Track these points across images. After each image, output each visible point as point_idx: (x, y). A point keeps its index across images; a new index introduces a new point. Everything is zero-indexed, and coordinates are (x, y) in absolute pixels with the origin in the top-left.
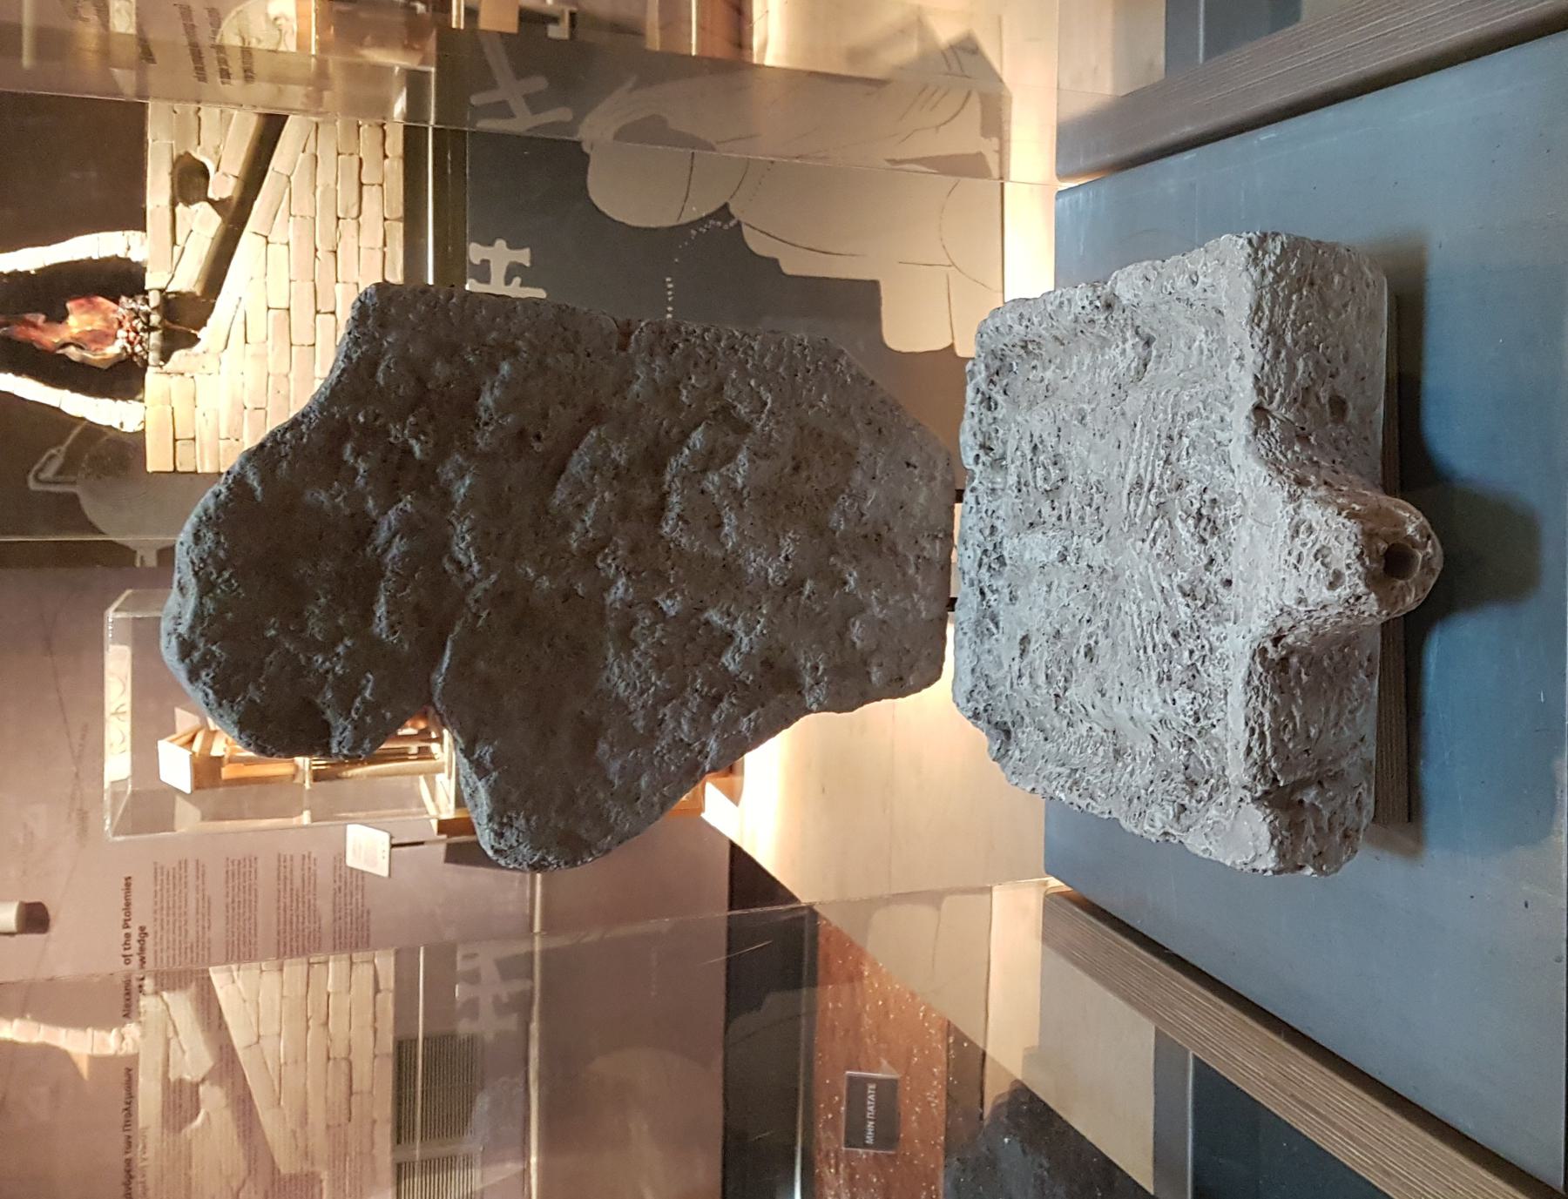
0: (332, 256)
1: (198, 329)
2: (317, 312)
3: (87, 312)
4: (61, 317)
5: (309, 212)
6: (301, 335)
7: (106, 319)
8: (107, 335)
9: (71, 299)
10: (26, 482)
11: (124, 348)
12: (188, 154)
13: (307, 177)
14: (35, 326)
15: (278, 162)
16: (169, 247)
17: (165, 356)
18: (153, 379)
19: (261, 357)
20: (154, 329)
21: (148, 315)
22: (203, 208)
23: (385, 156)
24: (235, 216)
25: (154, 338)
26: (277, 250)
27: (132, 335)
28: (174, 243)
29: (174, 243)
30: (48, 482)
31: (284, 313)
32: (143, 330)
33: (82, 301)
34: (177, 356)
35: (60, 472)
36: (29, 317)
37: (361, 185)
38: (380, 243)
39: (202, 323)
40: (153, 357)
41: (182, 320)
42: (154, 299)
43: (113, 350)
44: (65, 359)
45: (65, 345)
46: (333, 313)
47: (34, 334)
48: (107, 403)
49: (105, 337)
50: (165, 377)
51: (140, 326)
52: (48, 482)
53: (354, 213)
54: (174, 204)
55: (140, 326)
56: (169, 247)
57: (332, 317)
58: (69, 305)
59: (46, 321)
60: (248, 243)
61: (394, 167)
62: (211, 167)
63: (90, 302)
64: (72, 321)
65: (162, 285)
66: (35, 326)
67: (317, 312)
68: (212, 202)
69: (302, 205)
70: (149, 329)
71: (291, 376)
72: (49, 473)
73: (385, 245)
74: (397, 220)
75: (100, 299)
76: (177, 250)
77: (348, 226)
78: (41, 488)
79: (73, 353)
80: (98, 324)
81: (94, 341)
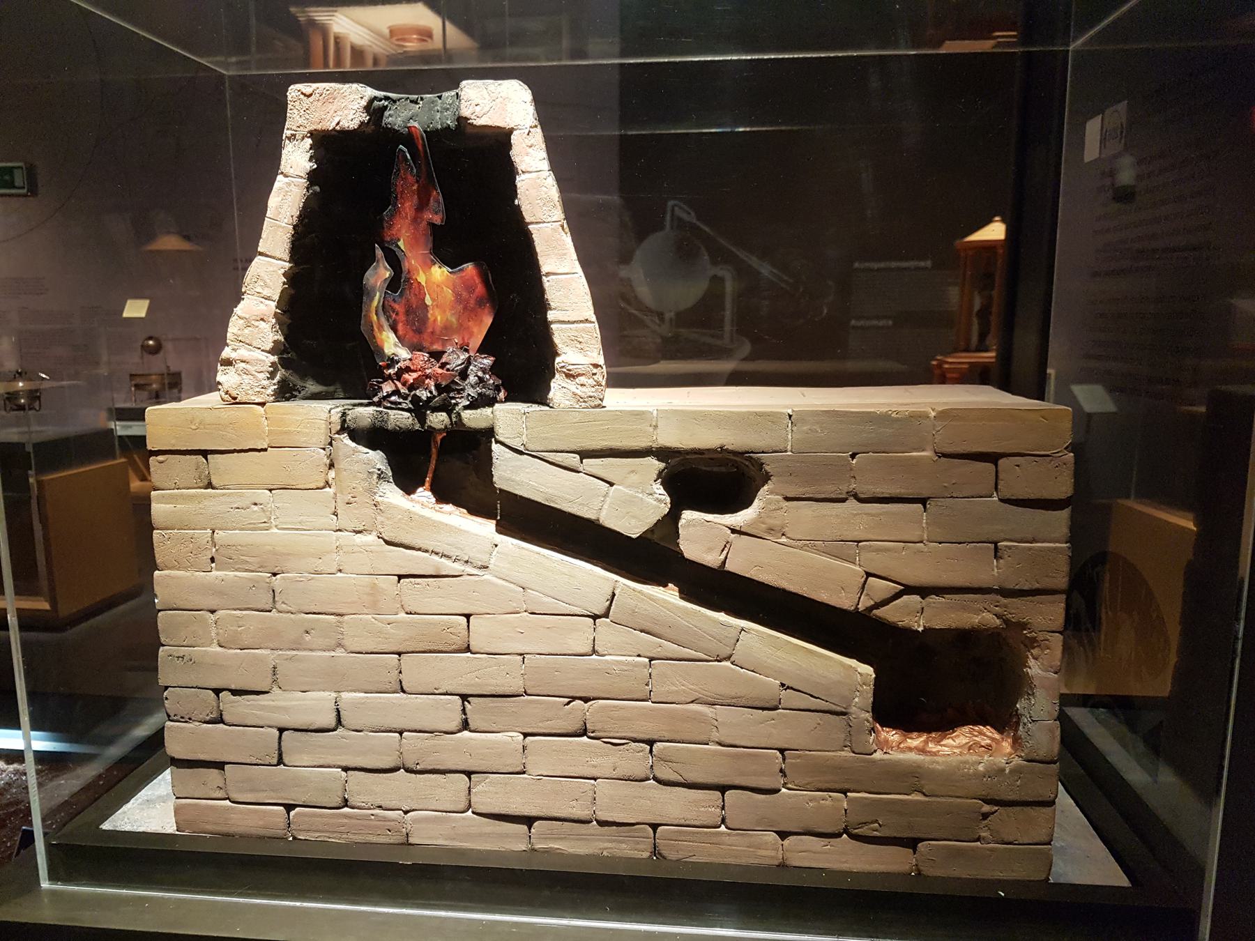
0: (576, 726)
1: (434, 490)
2: (464, 697)
3: (458, 296)
4: (447, 249)
5: (659, 691)
6: (417, 670)
7: (447, 328)
8: (419, 331)
9: (478, 266)
10: (675, 199)
11: (392, 361)
12: (767, 478)
13: (732, 691)
14: (422, 206)
15: (756, 638)
16: (599, 423)
17: (372, 437)
18: (318, 415)
19: (374, 603)
20: (422, 418)
21: (447, 408)
22: (657, 502)
23: (783, 835)
24: (649, 557)
25: (401, 418)
26: (579, 636)
27: (410, 377)
28: (585, 454)
29: (585, 454)
30: (673, 211)
31: (459, 642)
32: (416, 400)
33: (480, 289)
34: (377, 458)
35: (680, 219)
36: (437, 196)
37: (723, 789)
38: (603, 816)
39: (442, 496)
40: (364, 414)
41: (442, 461)
42: (474, 418)
43: (390, 344)
44: (368, 260)
45: (394, 261)
46: (465, 725)
47: (408, 206)
48: (269, 334)
49: (415, 328)
50: (323, 439)
51: (424, 395)
52: (673, 211)
53: (665, 773)
54: (662, 453)
55: (424, 395)
56: (599, 423)
57: (455, 723)
58: (469, 267)
59: (432, 225)
60: (590, 580)
61: (762, 850)
62: (740, 518)
63: (480, 303)
64: (439, 273)
65: (501, 433)
66: (422, 206)
67: (464, 697)
68: (672, 518)
69: (675, 680)
70: (419, 408)
71: (340, 653)
72: (677, 211)
73: (602, 823)
74: (655, 850)
75: (488, 321)
76: (573, 460)
77: (635, 759)
78: (669, 209)
79: (379, 274)
80: (438, 317)
81: (409, 311)
